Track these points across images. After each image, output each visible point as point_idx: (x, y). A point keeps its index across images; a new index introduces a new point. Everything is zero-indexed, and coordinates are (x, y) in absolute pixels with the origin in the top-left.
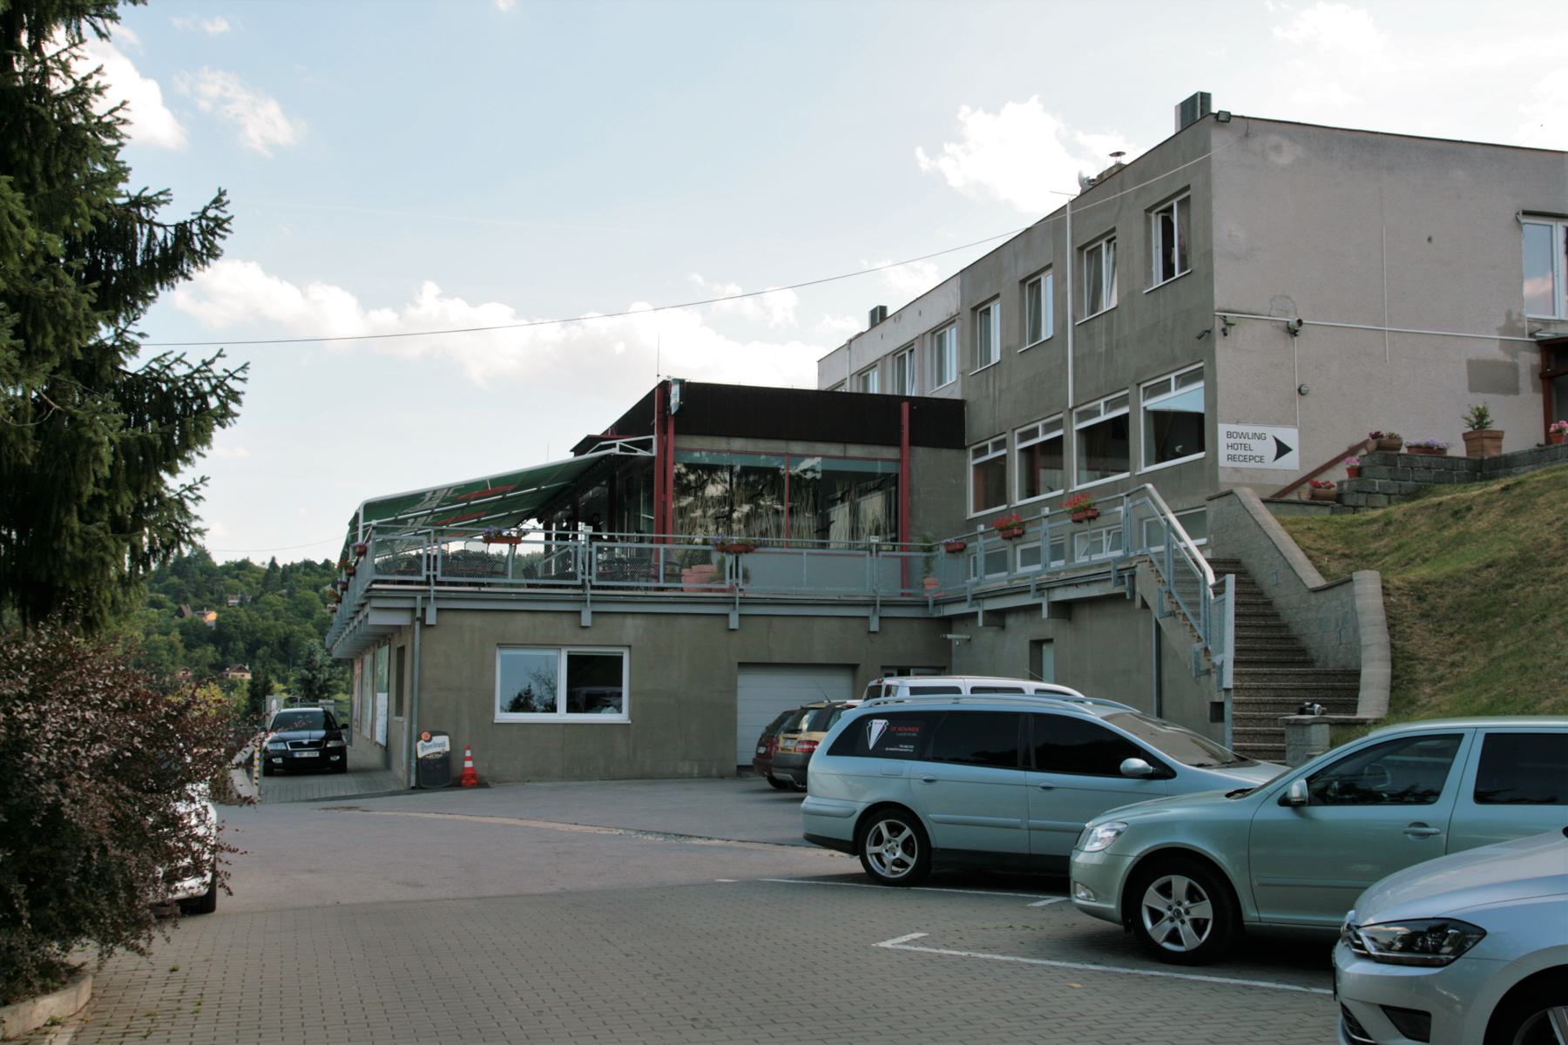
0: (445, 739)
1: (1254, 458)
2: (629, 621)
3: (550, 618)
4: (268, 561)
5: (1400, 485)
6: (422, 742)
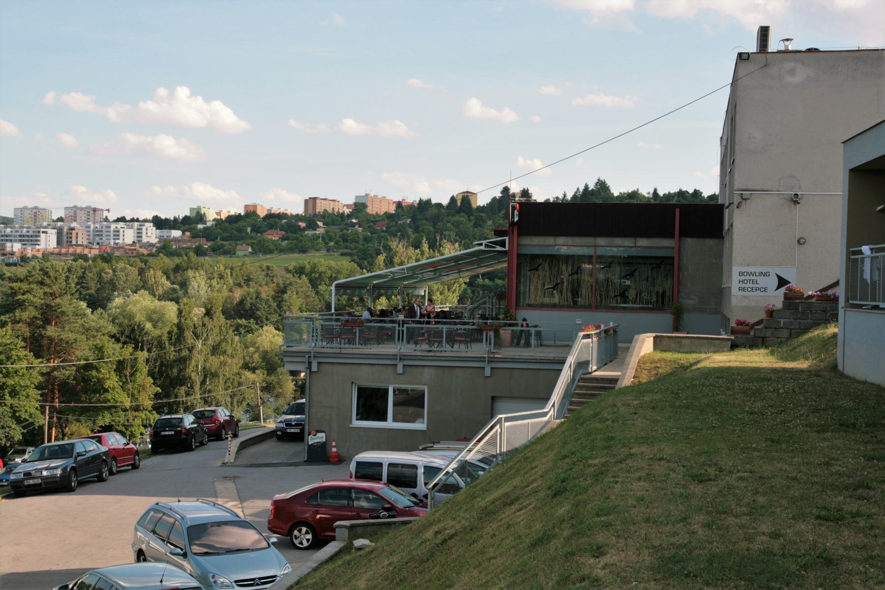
0: (324, 435)
1: (760, 289)
2: (426, 370)
3: (381, 368)
4: (652, 191)
5: (800, 323)
6: (311, 436)
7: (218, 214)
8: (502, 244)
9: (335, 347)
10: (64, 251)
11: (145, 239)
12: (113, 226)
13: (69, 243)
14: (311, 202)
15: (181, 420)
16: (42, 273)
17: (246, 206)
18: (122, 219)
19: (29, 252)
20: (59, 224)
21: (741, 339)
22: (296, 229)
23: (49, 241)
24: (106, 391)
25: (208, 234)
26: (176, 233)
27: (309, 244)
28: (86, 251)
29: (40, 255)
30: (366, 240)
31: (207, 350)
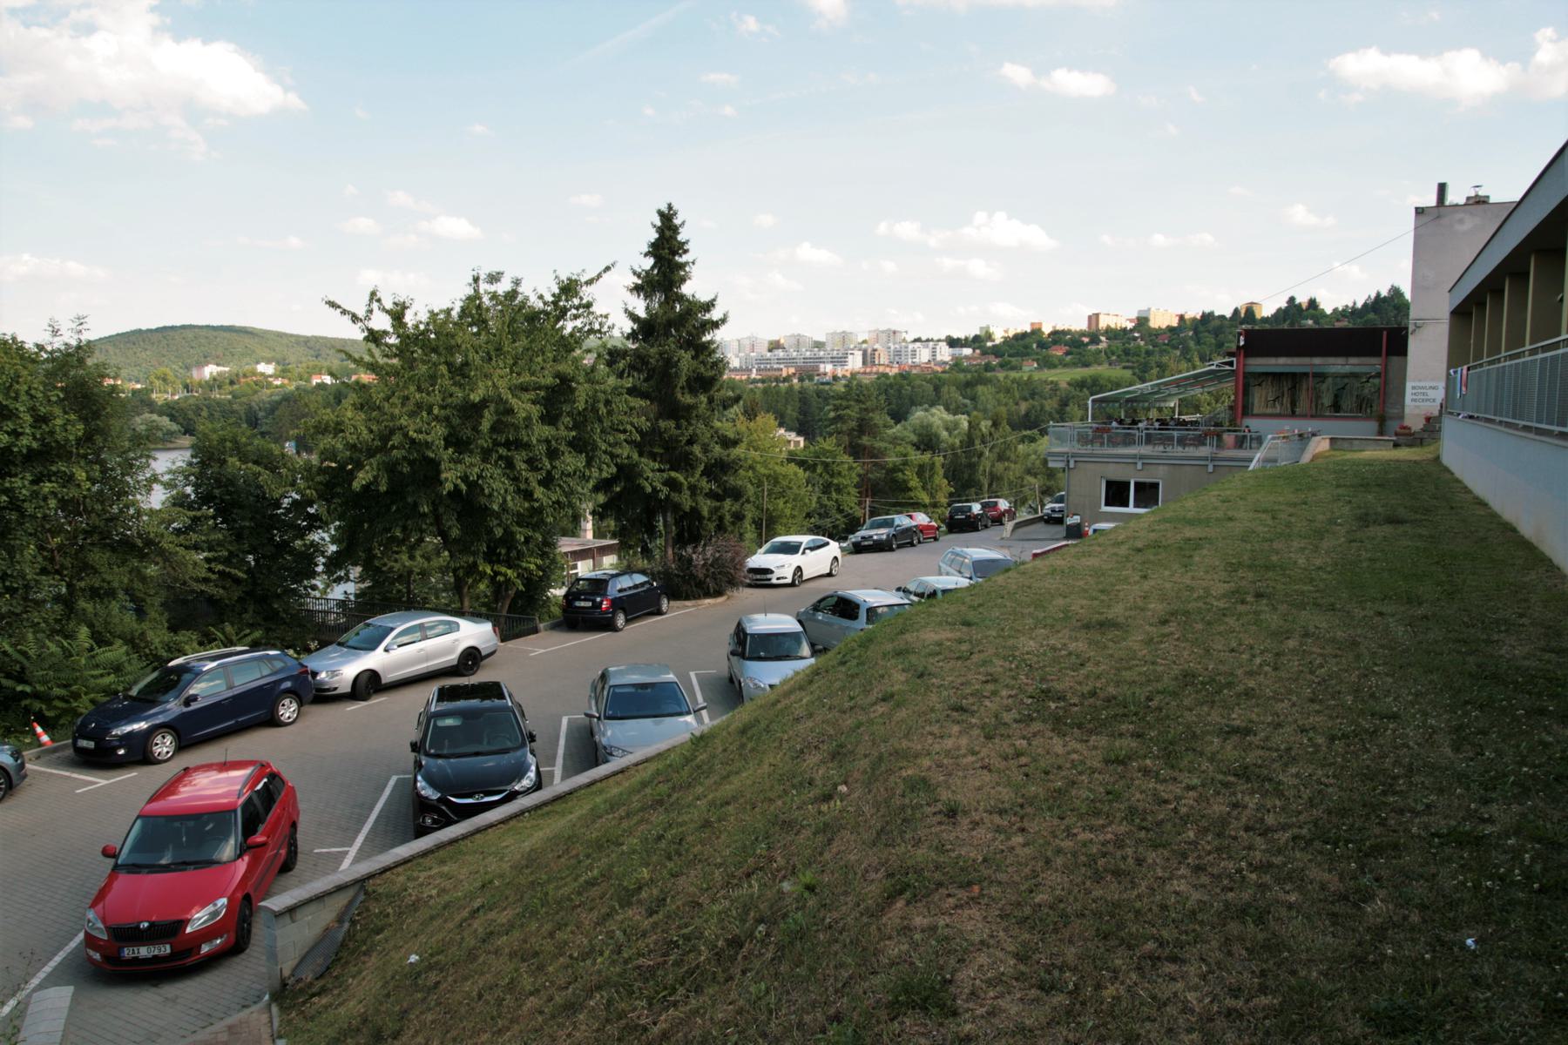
2: (1161, 467)
7: (1006, 331)
8: (1231, 364)
9: (1088, 449)
10: (868, 370)
11: (939, 358)
12: (911, 346)
13: (873, 364)
14: (1093, 319)
15: (970, 508)
16: (607, 357)
17: (1032, 324)
18: (918, 340)
19: (840, 373)
20: (864, 346)
21: (1402, 439)
22: (1081, 345)
23: (855, 363)
24: (910, 489)
25: (996, 351)
26: (967, 351)
27: (1092, 359)
28: (888, 370)
29: (848, 375)
30: (1148, 353)
31: (993, 456)
